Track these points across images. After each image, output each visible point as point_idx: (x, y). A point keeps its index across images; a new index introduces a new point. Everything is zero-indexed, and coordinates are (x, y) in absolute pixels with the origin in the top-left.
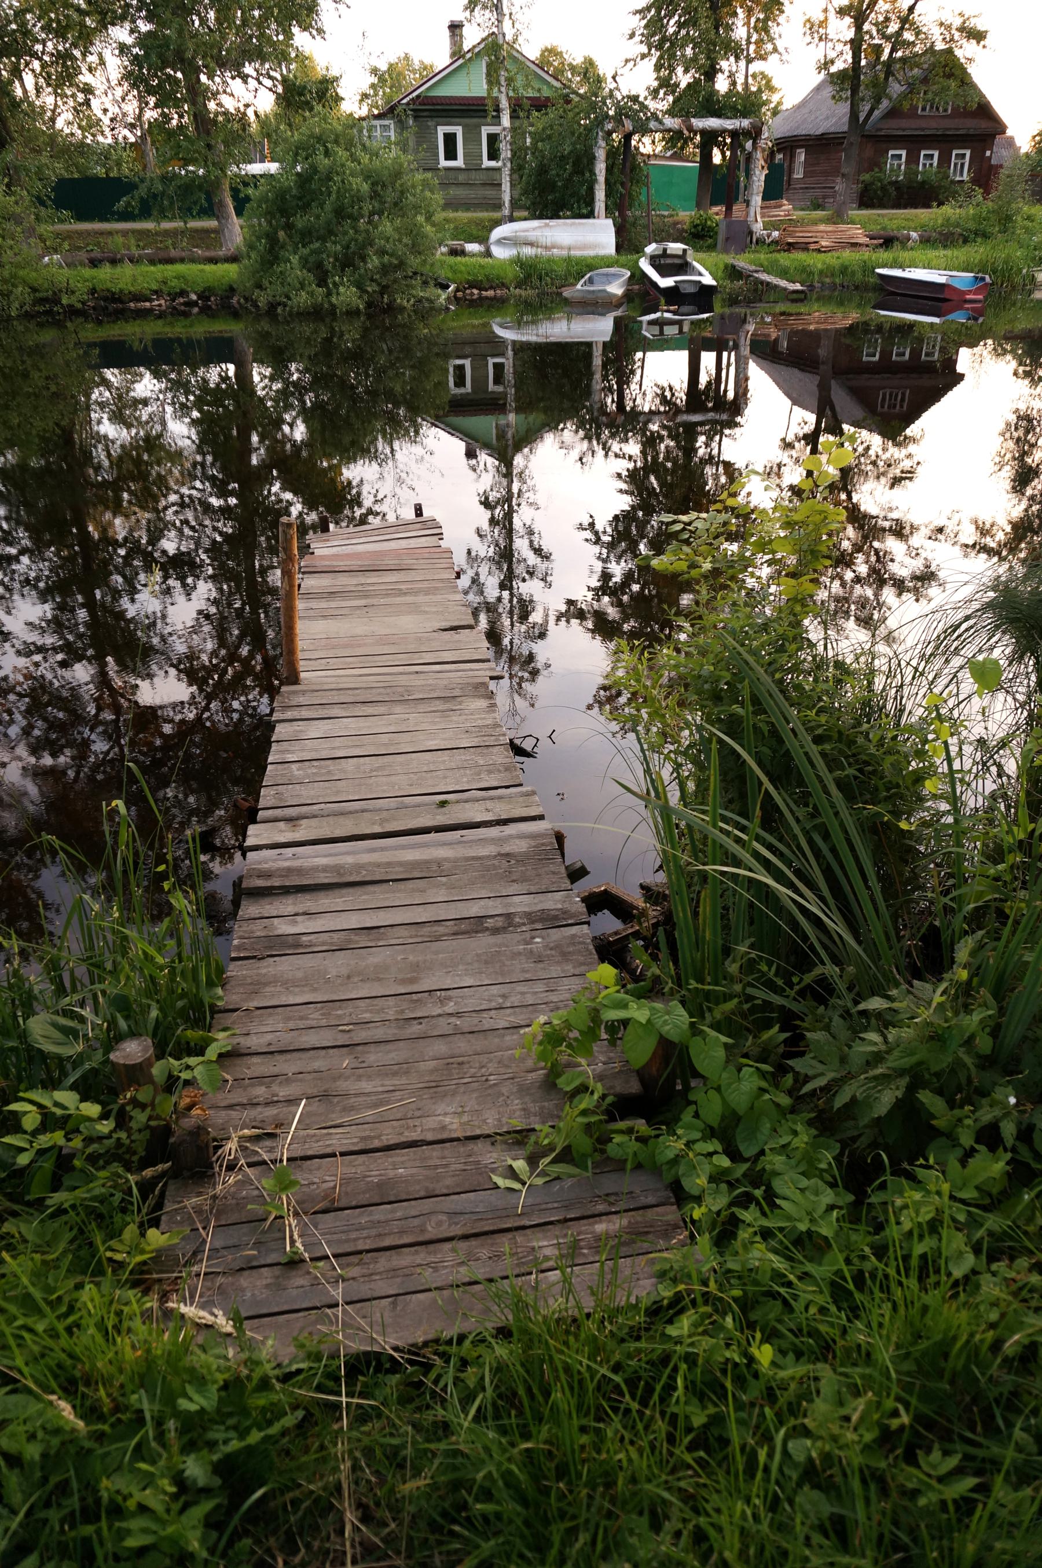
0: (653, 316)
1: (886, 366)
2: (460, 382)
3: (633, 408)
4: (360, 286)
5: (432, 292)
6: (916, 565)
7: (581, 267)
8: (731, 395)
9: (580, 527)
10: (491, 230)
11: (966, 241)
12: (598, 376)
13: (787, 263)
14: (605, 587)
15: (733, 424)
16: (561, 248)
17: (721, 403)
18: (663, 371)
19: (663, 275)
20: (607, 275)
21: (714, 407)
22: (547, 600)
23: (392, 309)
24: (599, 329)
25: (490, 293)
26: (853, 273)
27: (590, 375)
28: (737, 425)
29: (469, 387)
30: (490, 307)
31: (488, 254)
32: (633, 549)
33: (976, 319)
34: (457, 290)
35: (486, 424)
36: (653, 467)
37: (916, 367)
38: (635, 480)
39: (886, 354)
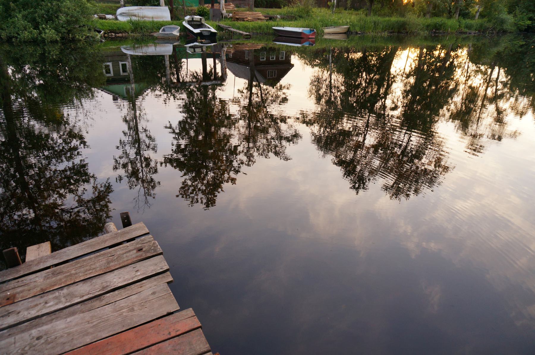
0: (192, 44)
1: (268, 63)
2: (108, 72)
3: (183, 80)
4: (56, 29)
5: (93, 33)
6: (292, 132)
7: (158, 26)
8: (220, 74)
9: (166, 127)
10: (116, 10)
11: (296, 19)
12: (168, 68)
13: (239, 25)
14: (179, 149)
15: (221, 85)
16: (149, 18)
17: (216, 78)
18: (193, 66)
19: (195, 28)
20: (171, 28)
21: (211, 80)
22: (156, 157)
23: (74, 40)
24: (167, 50)
25: (120, 35)
26: (264, 29)
27: (166, 68)
28: (223, 85)
29: (112, 74)
30: (120, 41)
31: (116, 19)
32: (188, 133)
33: (312, 45)
34: (105, 33)
35: (122, 88)
36: (192, 103)
37: (278, 62)
38: (187, 108)
39: (268, 58)
